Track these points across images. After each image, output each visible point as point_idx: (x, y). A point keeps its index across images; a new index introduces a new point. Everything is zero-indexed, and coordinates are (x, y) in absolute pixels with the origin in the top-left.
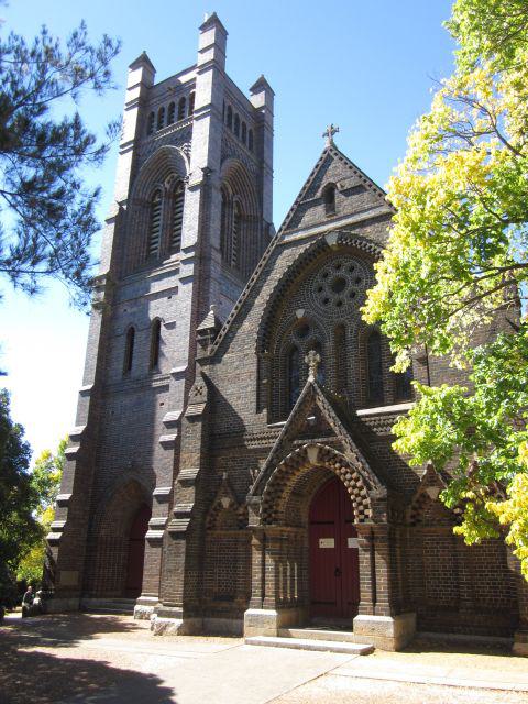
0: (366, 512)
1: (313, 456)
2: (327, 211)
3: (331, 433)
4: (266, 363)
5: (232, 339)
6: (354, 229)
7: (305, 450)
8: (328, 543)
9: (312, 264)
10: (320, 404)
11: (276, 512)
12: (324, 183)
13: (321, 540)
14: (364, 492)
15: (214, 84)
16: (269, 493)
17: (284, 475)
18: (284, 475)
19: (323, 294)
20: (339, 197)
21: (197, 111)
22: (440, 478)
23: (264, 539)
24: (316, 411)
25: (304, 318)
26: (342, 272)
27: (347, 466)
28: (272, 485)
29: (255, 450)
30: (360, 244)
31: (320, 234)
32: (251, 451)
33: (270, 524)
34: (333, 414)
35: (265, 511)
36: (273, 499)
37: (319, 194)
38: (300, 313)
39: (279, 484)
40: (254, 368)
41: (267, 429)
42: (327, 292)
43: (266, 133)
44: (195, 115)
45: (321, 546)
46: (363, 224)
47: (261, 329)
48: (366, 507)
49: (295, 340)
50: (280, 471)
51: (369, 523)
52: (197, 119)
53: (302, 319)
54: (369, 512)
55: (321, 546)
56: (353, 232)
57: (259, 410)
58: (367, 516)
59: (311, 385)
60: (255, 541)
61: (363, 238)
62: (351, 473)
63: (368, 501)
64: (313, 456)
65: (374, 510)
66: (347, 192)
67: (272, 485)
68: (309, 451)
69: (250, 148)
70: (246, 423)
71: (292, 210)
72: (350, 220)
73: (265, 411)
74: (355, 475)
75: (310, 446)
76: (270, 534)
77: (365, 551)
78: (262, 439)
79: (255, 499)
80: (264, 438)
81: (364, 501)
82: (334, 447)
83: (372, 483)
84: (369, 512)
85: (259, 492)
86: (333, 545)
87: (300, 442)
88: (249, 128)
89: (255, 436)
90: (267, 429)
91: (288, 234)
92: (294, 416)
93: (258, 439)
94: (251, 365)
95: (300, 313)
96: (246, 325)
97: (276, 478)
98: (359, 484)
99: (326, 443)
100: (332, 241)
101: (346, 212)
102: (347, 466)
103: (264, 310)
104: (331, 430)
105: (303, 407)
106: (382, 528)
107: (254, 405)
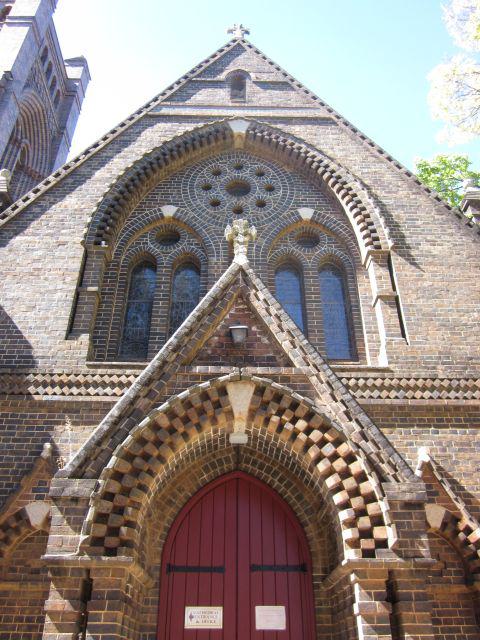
0: (378, 532)
1: (241, 399)
2: (233, 96)
3: (277, 358)
4: (96, 263)
5: (36, 216)
6: (276, 123)
7: (223, 391)
8: (203, 617)
9: (207, 147)
10: (259, 306)
11: (130, 524)
12: (231, 68)
13: (189, 610)
14: (371, 485)
15: (21, 51)
16: (117, 476)
17: (162, 436)
18: (162, 436)
19: (212, 194)
20: (249, 87)
21: (10, 18)
22: (447, 488)
23: (86, 595)
24: (251, 315)
25: (175, 218)
26: (245, 174)
27: (325, 428)
28: (128, 457)
29: (50, 406)
30: (285, 141)
31: (220, 117)
32: (42, 404)
33: (111, 552)
34: (289, 325)
35: (100, 518)
36: (126, 492)
37: (222, 77)
38: (169, 211)
39: (146, 457)
40: (77, 265)
41: (85, 369)
42: (219, 193)
43: (74, 105)
44: (7, 21)
45: (189, 624)
46: (288, 121)
47: (105, 200)
48: (378, 521)
49: (155, 249)
50: (155, 427)
51: (386, 558)
52: (9, 24)
53: (170, 218)
54: (389, 533)
55: (189, 624)
56: (273, 126)
57: (71, 332)
58: (383, 544)
59: (241, 270)
60: (56, 602)
61: (293, 137)
62: (338, 443)
63: (382, 506)
64: (241, 399)
65: (398, 526)
66: (265, 85)
67: (128, 457)
68: (231, 389)
69: (56, 102)
70: (37, 352)
71: (178, 83)
72: (270, 113)
73: (85, 338)
74: (344, 449)
75: (239, 379)
76: (102, 583)
77: (60, 628)
78: (70, 385)
79: (78, 487)
80: (78, 385)
81: (371, 508)
82: (294, 387)
83: (385, 467)
84: (389, 533)
85: (89, 469)
86: (189, 610)
87: (211, 369)
88: (58, 87)
89: (56, 379)
90: (85, 369)
91: (167, 106)
92: (199, 318)
93: (62, 385)
94: (71, 259)
95: (169, 211)
96: (71, 201)
97: (141, 441)
98: (355, 468)
99: (275, 378)
100: (239, 128)
101: (262, 103)
102: (325, 428)
103: (111, 186)
104: (279, 350)
105: (206, 320)
106: (423, 570)
107: (64, 324)
